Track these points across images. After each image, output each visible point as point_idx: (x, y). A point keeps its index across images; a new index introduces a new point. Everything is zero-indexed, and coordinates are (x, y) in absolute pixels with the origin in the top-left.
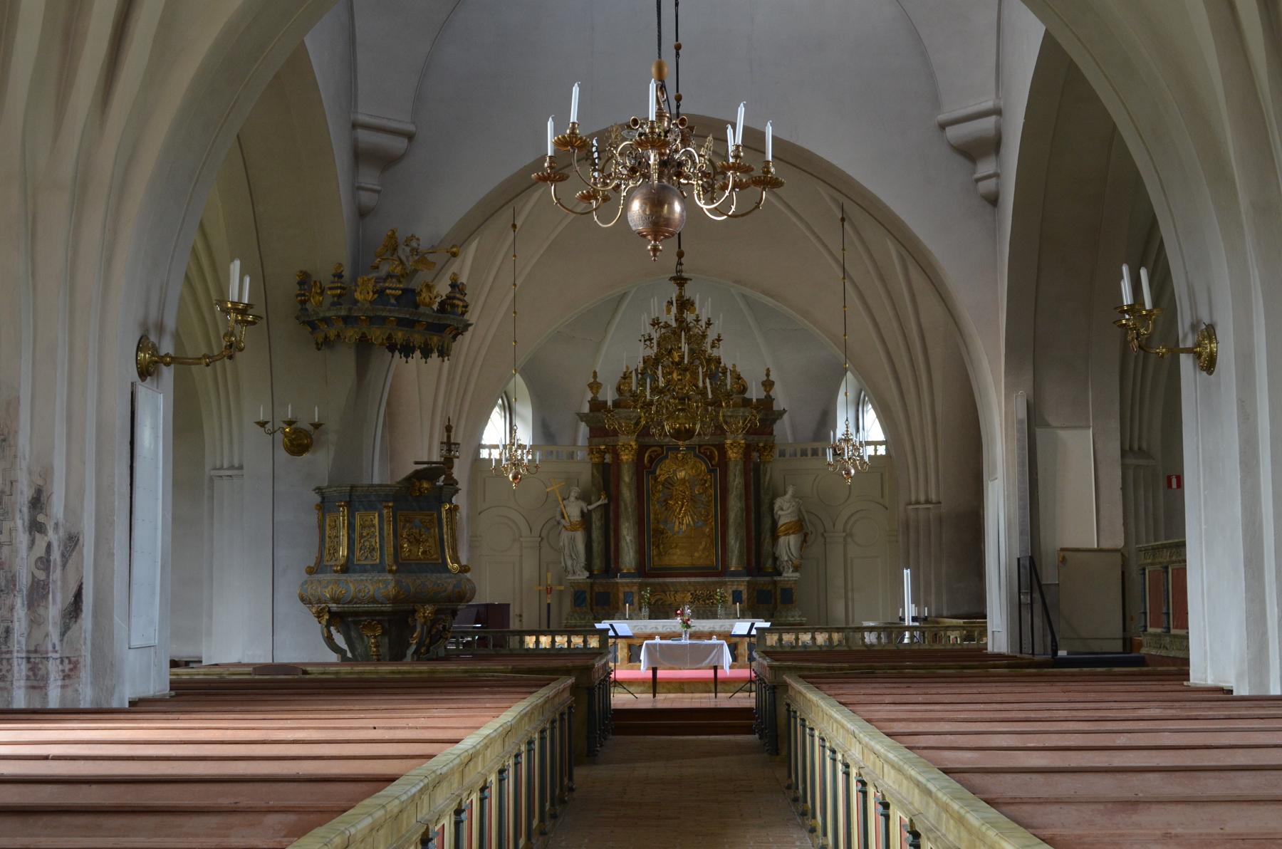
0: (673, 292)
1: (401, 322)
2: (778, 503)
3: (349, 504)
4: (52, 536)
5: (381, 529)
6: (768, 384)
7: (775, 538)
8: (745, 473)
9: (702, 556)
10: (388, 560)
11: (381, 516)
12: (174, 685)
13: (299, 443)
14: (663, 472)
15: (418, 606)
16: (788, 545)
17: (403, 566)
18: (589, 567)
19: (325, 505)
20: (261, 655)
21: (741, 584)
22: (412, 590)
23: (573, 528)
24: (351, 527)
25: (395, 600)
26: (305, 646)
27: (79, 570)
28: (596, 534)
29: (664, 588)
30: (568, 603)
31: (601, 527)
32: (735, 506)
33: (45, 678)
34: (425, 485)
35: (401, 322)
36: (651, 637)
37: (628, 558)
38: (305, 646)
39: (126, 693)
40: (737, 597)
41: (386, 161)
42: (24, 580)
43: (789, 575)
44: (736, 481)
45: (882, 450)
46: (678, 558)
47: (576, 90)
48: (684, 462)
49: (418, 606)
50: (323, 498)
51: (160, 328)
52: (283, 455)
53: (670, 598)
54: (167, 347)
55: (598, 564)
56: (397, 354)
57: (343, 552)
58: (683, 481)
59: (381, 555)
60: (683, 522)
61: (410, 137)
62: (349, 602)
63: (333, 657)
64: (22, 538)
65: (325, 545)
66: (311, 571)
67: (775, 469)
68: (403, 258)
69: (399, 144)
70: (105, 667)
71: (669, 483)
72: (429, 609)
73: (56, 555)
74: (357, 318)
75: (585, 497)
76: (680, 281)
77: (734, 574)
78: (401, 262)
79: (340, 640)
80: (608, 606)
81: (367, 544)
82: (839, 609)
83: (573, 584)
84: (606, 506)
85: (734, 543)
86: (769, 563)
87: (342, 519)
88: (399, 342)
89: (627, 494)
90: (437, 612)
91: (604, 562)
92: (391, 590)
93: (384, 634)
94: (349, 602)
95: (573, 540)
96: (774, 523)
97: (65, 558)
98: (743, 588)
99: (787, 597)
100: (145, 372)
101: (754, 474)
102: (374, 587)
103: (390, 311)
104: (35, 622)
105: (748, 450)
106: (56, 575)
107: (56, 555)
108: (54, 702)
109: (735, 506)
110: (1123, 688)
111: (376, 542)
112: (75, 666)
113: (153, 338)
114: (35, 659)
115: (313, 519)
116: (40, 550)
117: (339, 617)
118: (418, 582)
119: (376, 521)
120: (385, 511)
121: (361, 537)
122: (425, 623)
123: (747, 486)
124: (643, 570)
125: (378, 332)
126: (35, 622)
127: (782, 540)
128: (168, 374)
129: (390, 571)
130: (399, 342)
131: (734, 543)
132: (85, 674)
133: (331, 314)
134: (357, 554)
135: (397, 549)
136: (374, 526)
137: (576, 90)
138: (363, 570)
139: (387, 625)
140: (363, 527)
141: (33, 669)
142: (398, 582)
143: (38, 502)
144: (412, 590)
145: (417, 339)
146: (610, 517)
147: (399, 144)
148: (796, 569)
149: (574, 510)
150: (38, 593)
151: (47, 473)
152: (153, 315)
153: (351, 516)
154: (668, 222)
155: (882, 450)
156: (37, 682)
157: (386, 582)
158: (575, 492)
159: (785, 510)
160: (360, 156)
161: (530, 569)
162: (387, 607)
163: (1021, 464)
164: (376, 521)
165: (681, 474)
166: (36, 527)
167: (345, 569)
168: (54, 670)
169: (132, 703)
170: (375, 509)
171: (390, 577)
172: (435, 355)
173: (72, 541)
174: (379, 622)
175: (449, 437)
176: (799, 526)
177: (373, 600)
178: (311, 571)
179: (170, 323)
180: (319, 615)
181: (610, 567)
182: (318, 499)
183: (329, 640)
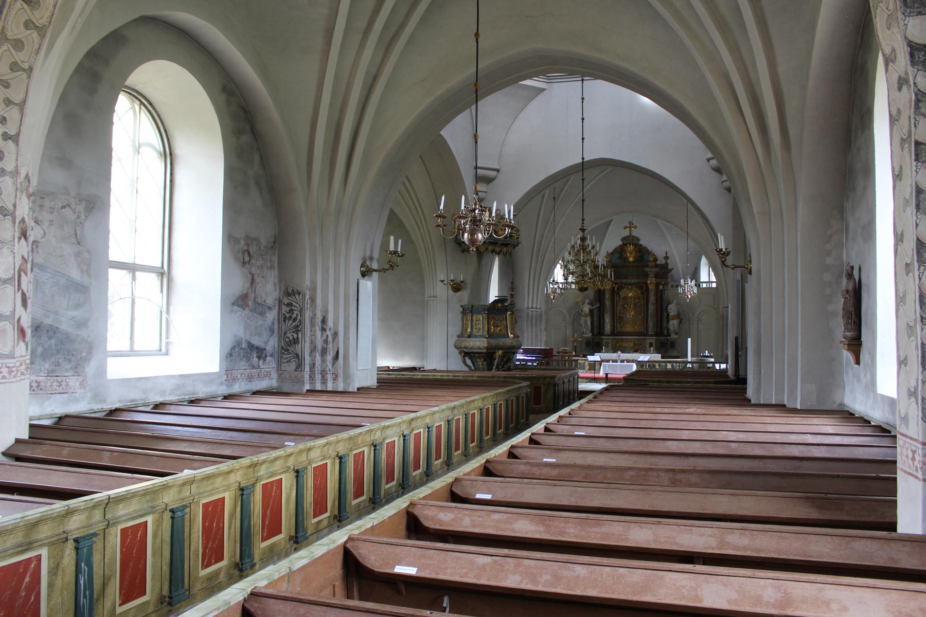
0: (580, 235)
2: (670, 306)
3: (471, 312)
4: (329, 333)
6: (666, 258)
7: (668, 321)
8: (656, 294)
9: (637, 328)
10: (485, 333)
12: (379, 381)
14: (623, 293)
16: (673, 324)
17: (490, 335)
18: (592, 332)
19: (464, 312)
20: (441, 366)
21: (653, 340)
23: (586, 316)
24: (472, 320)
25: (487, 348)
26: (456, 365)
27: (338, 344)
28: (595, 319)
29: (622, 340)
30: (584, 345)
31: (597, 315)
32: (651, 308)
33: (326, 380)
36: (608, 361)
37: (608, 328)
38: (456, 365)
39: (353, 387)
40: (651, 345)
41: (489, 180)
42: (319, 347)
43: (673, 336)
44: (652, 298)
45: (714, 285)
46: (629, 328)
47: (443, 198)
48: (631, 290)
51: (371, 259)
52: (451, 292)
53: (625, 344)
54: (375, 266)
55: (596, 331)
57: (469, 330)
58: (631, 297)
60: (630, 314)
61: (498, 171)
63: (466, 369)
64: (319, 333)
65: (464, 329)
66: (458, 336)
67: (669, 293)
69: (493, 173)
70: (347, 377)
71: (625, 298)
72: (500, 352)
73: (330, 339)
75: (591, 304)
76: (583, 230)
77: (651, 335)
79: (469, 362)
80: (595, 347)
83: (586, 338)
84: (599, 308)
85: (651, 324)
86: (666, 331)
87: (469, 318)
89: (608, 303)
90: (504, 353)
91: (598, 329)
92: (485, 345)
95: (586, 322)
96: (668, 315)
97: (333, 340)
98: (653, 341)
99: (673, 345)
100: (364, 275)
101: (660, 295)
102: (479, 343)
104: (324, 361)
105: (657, 285)
106: (330, 345)
107: (330, 339)
108: (330, 388)
109: (651, 308)
110: (703, 411)
112: (337, 376)
113: (368, 263)
114: (323, 373)
115: (460, 316)
116: (324, 338)
117: (467, 354)
123: (657, 300)
124: (613, 333)
126: (324, 361)
127: (671, 322)
128: (375, 274)
131: (651, 324)
132: (340, 379)
135: (489, 329)
137: (443, 198)
138: (476, 336)
141: (323, 377)
143: (324, 321)
145: (497, 249)
146: (601, 311)
147: (493, 173)
148: (676, 334)
149: (586, 309)
150: (324, 352)
151: (326, 311)
152: (368, 254)
153: (472, 316)
154: (476, 240)
155: (714, 285)
156: (324, 381)
158: (587, 301)
159: (672, 310)
160: (479, 179)
161: (569, 331)
162: (485, 351)
163: (738, 298)
165: (630, 295)
166: (323, 330)
167: (469, 336)
168: (329, 377)
169: (358, 389)
173: (336, 334)
176: (678, 316)
177: (479, 348)
178: (458, 336)
179: (376, 255)
180: (460, 353)
181: (601, 332)
183: (464, 362)
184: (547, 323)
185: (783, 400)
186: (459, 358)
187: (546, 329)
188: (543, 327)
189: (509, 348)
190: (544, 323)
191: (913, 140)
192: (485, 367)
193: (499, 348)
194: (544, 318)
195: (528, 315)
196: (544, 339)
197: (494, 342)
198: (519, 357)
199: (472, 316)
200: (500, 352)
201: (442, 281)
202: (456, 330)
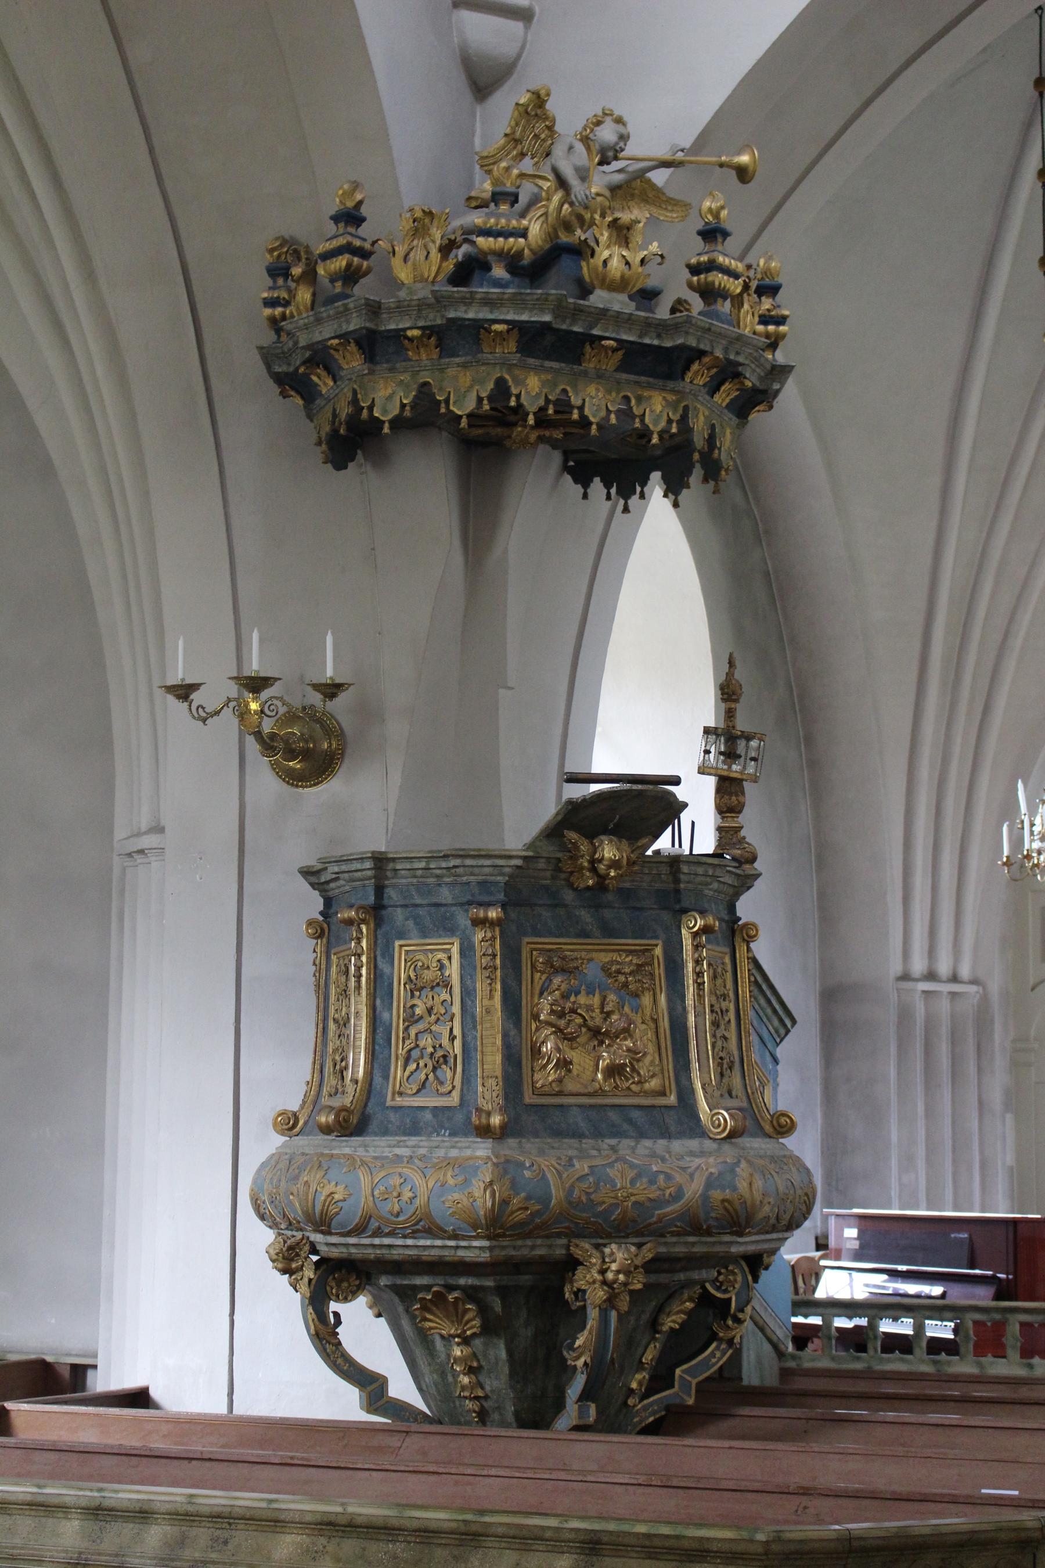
1: (533, 341)
5: (468, 993)
10: (488, 1094)
11: (466, 952)
13: (308, 748)
15: (583, 1248)
22: (556, 1194)
24: (380, 987)
25: (495, 1225)
34: (609, 851)
35: (533, 341)
49: (583, 1248)
50: (328, 902)
52: (265, 781)
56: (597, 486)
59: (467, 1079)
62: (359, 1230)
63: (343, 1403)
68: (568, 172)
74: (398, 335)
78: (562, 183)
81: (426, 1041)
82: (709, 947)
88: (531, 407)
92: (478, 1195)
93: (489, 1329)
94: (359, 1230)
102: (439, 1182)
103: (488, 302)
111: (449, 1032)
118: (582, 1167)
119: (447, 964)
120: (479, 935)
121: (412, 1019)
122: (611, 1301)
125: (465, 379)
129: (484, 1131)
130: (531, 407)
133: (325, 332)
134: (398, 1072)
135: (516, 1061)
136: (446, 984)
138: (412, 1124)
139: (497, 1305)
140: (415, 987)
142: (504, 1168)
144: (556, 1194)
157: (465, 1168)
162: (476, 1249)
164: (454, 971)
170: (451, 930)
171: (482, 1149)
172: (697, 475)
174: (471, 1294)
175: (730, 714)
182: (316, 903)
183: (326, 1337)
184: (1017, 1065)
185: (836, 1222)
186: (278, 1304)
187: (1014, 1100)
188: (996, 1096)
189: (694, 1224)
190: (1000, 1062)
191: (994, 1304)
192: (497, 1383)
193: (626, 1226)
194: (999, 1036)
195: (905, 1015)
196: (1005, 1157)
197: (557, 1169)
198: (838, 1283)
199: (382, 951)
200: (619, 1256)
201: (184, 692)
202: (283, 1078)
